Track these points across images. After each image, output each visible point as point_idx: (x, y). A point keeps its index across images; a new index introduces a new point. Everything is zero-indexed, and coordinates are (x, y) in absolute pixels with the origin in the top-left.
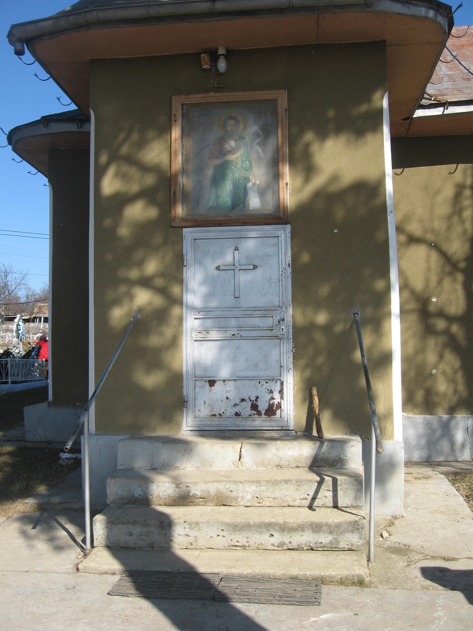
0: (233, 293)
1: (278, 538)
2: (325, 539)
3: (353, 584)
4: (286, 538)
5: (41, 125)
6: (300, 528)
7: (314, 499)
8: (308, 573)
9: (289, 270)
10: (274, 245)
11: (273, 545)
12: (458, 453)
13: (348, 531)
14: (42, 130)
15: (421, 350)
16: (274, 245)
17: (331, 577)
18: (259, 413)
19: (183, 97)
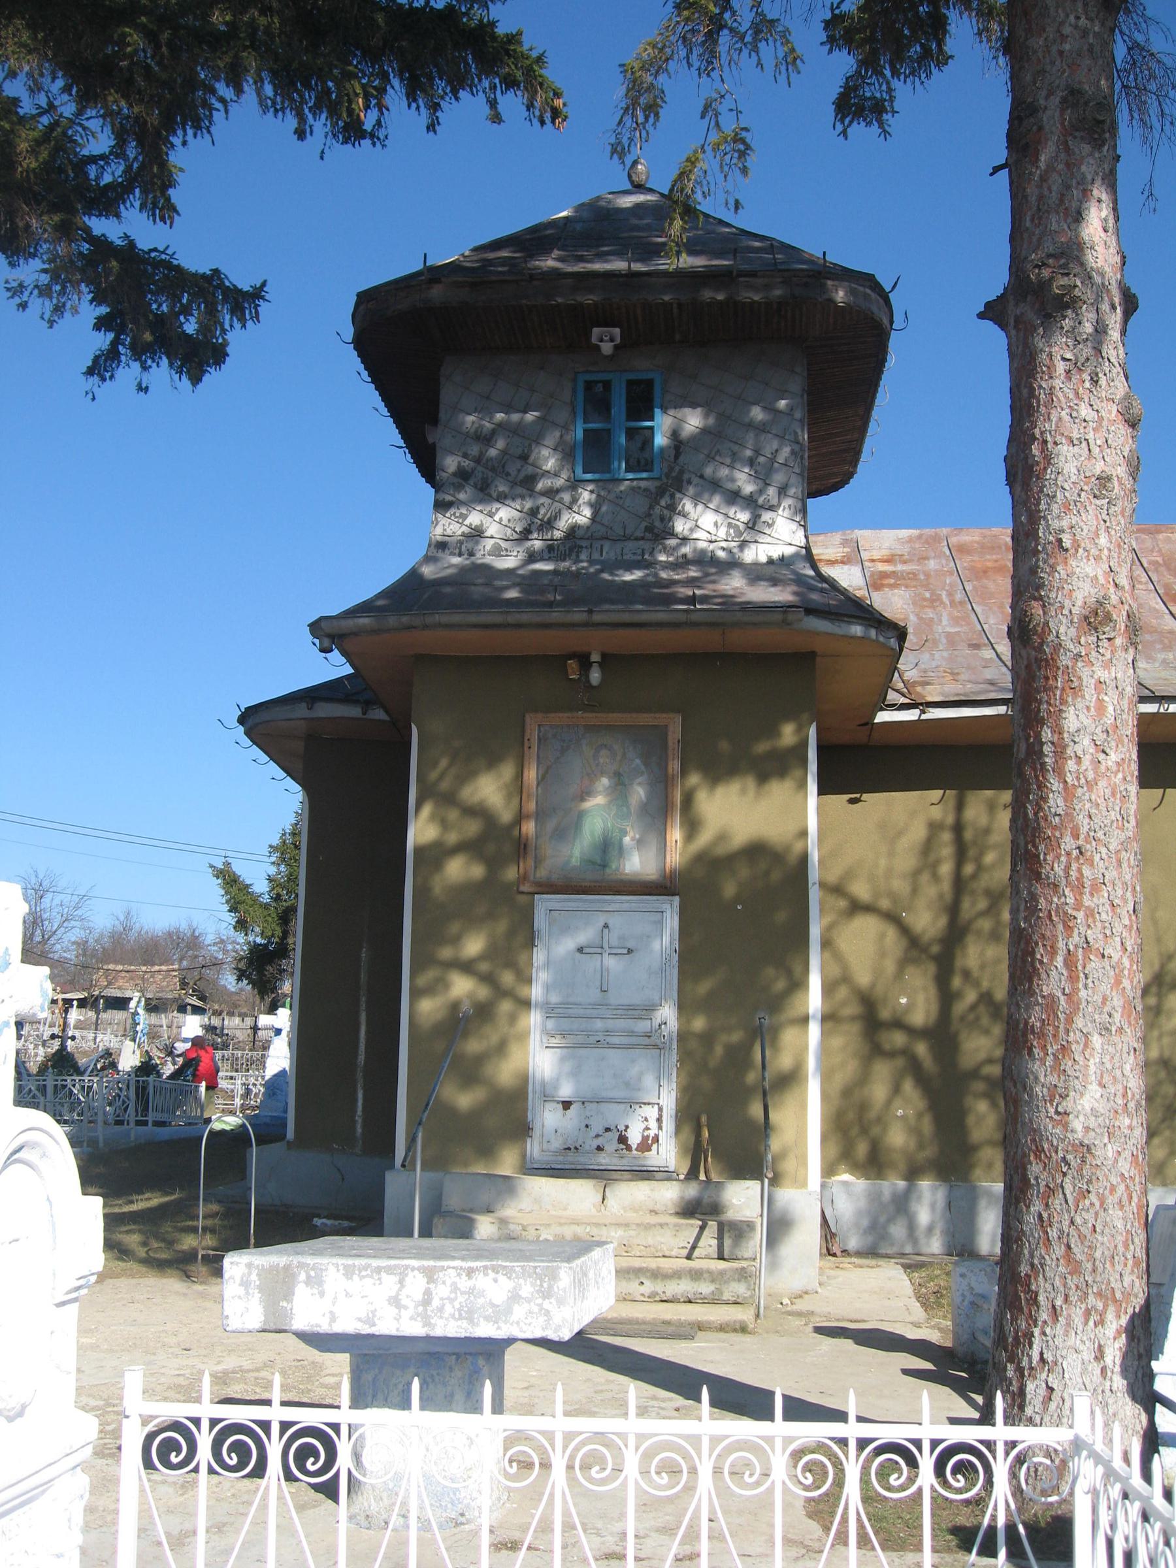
0: (598, 984)
1: (649, 1287)
2: (706, 1288)
3: (735, 1330)
4: (659, 1287)
5: (304, 705)
6: (677, 1275)
7: (694, 1247)
8: (683, 1318)
9: (676, 957)
10: (655, 922)
11: (643, 1295)
12: (922, 1240)
13: (734, 1280)
14: (302, 711)
15: (863, 1079)
16: (655, 922)
17: (709, 1322)
18: (629, 1148)
19: (540, 715)
